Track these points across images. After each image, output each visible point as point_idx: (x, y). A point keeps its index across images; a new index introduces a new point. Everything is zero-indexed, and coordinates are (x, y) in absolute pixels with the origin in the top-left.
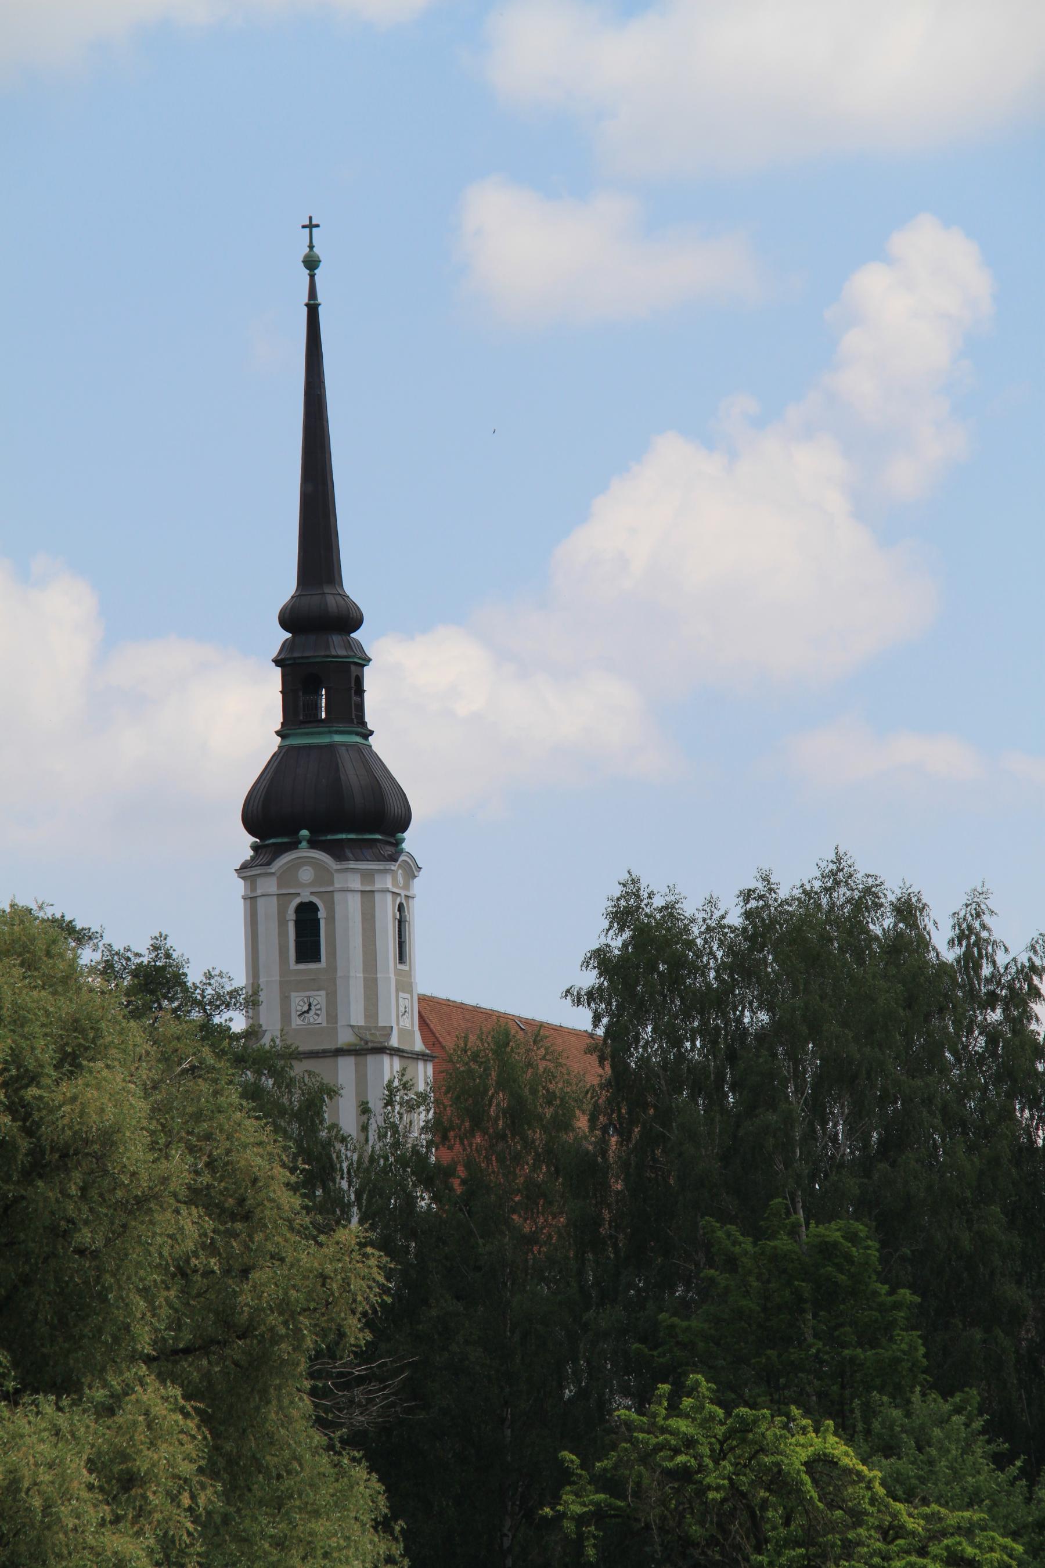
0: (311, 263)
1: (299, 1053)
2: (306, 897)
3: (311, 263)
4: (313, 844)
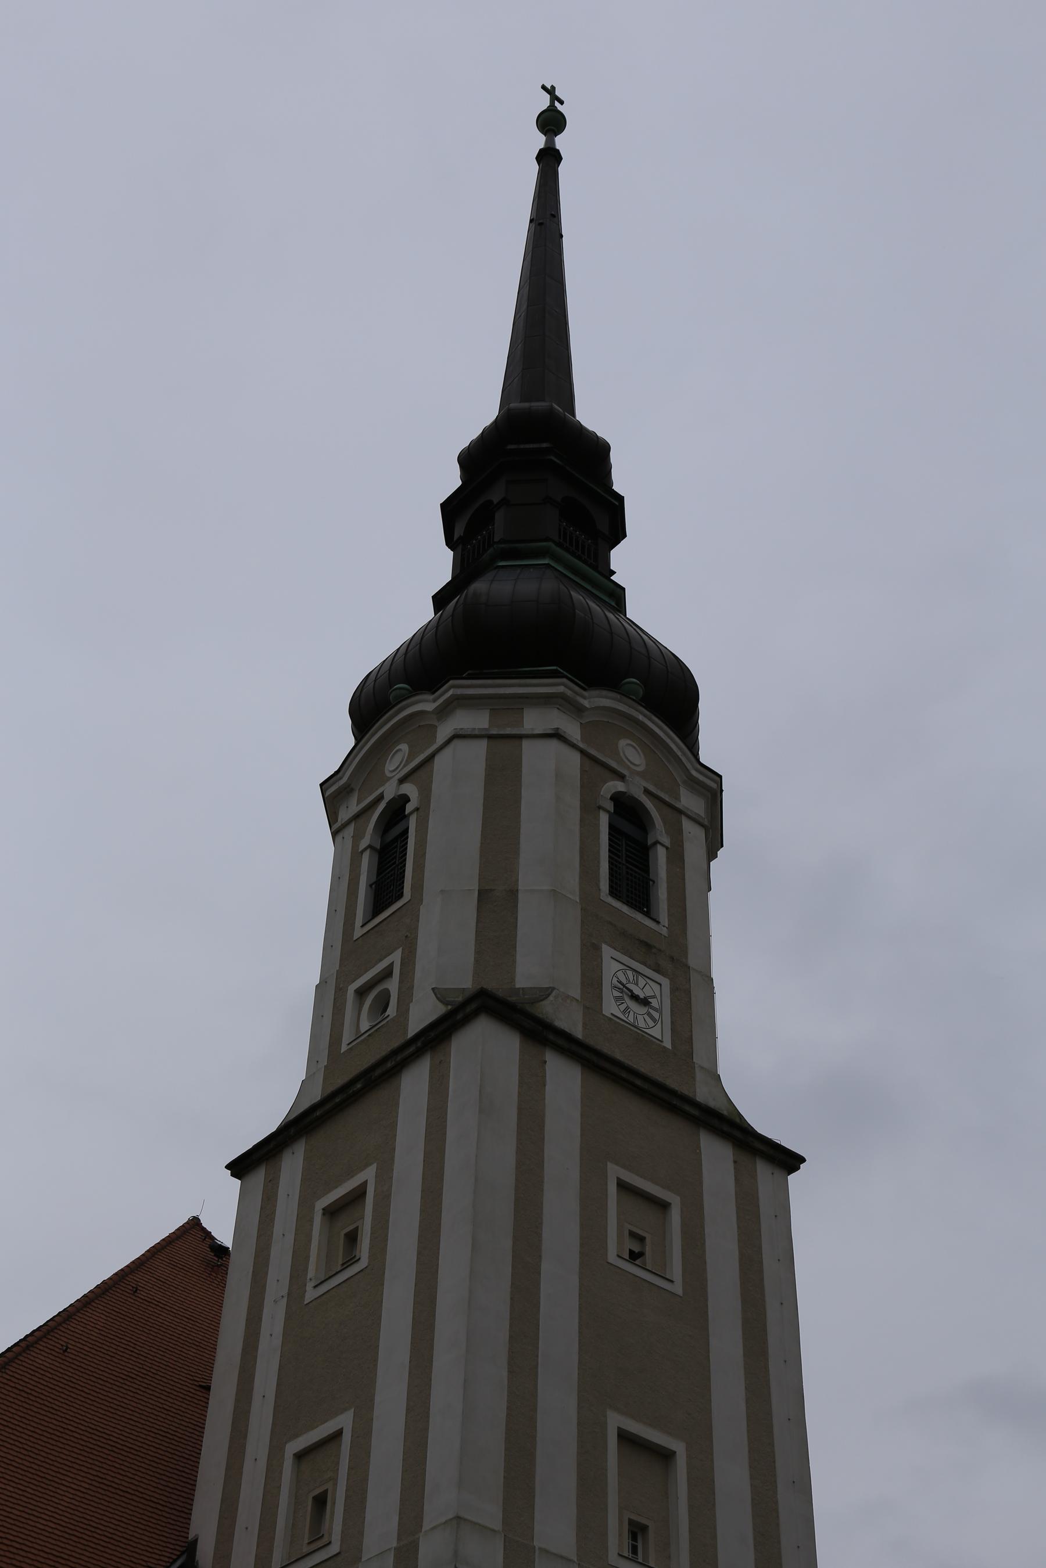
0: (551, 122)
3: (551, 122)
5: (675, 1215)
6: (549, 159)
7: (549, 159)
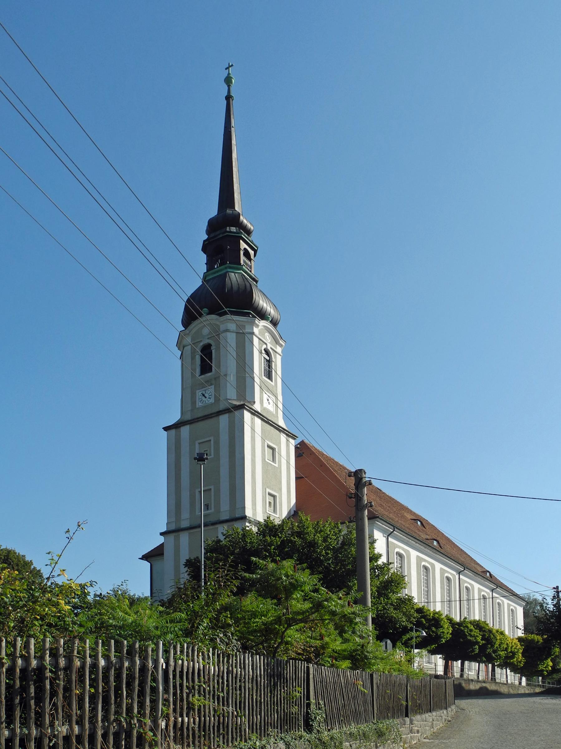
0: (228, 81)
1: (189, 424)
2: (206, 341)
3: (228, 81)
4: (210, 313)
5: (212, 442)
6: (229, 98)
7: (229, 98)
